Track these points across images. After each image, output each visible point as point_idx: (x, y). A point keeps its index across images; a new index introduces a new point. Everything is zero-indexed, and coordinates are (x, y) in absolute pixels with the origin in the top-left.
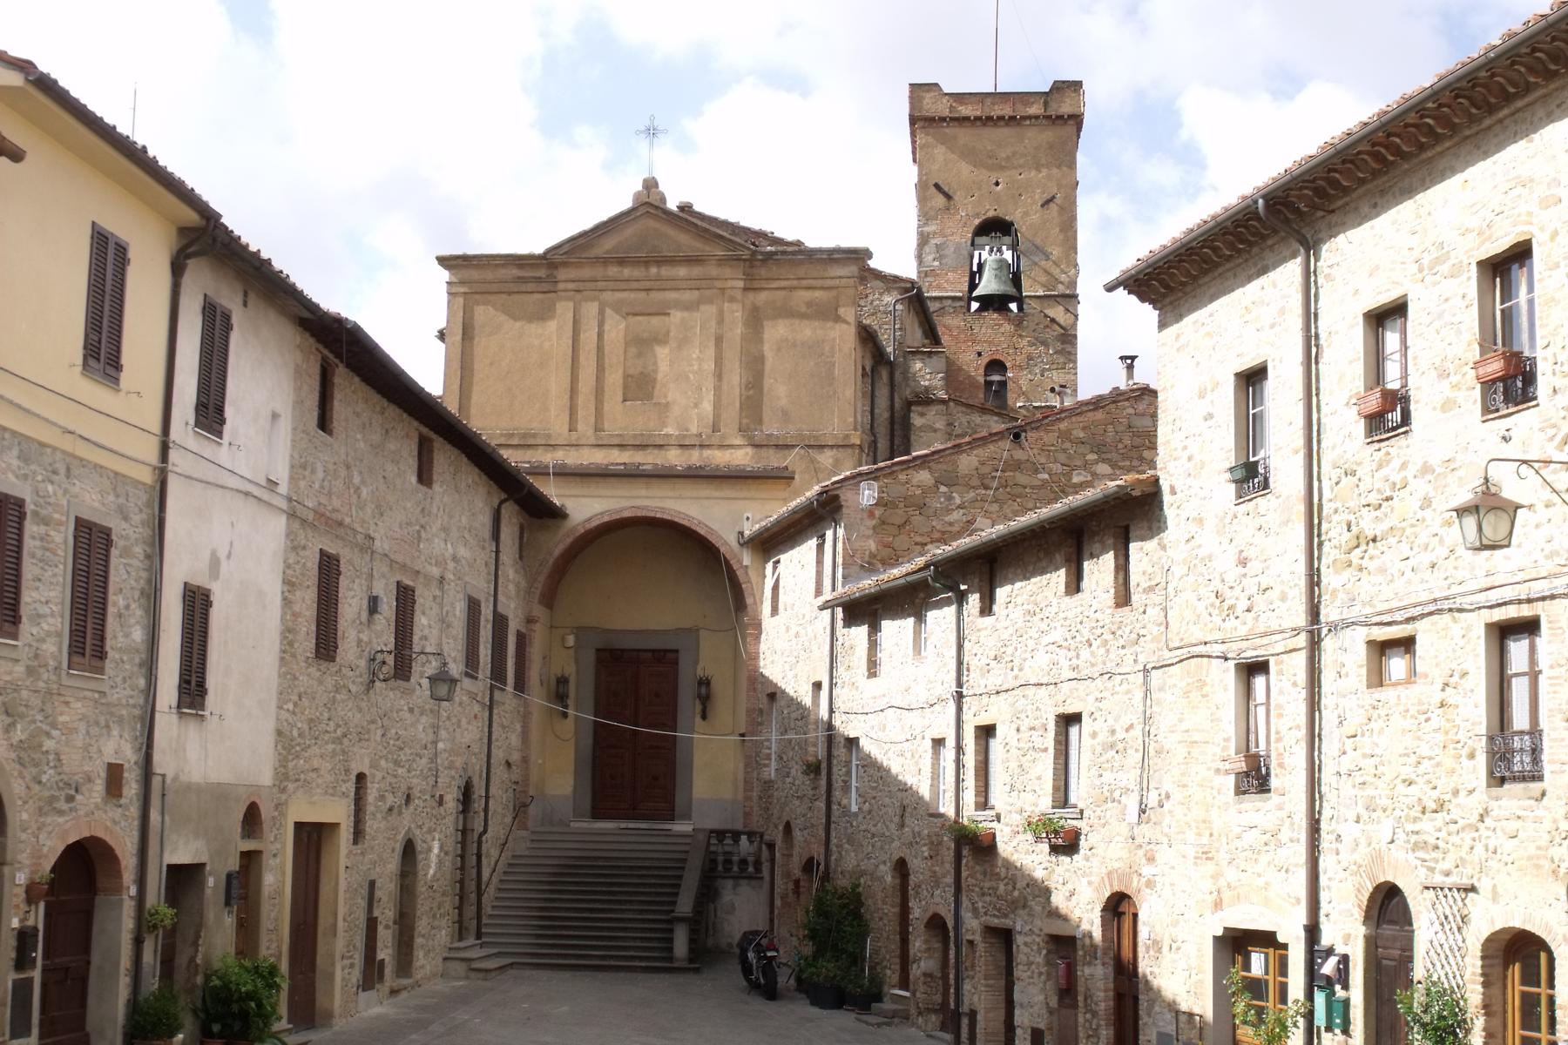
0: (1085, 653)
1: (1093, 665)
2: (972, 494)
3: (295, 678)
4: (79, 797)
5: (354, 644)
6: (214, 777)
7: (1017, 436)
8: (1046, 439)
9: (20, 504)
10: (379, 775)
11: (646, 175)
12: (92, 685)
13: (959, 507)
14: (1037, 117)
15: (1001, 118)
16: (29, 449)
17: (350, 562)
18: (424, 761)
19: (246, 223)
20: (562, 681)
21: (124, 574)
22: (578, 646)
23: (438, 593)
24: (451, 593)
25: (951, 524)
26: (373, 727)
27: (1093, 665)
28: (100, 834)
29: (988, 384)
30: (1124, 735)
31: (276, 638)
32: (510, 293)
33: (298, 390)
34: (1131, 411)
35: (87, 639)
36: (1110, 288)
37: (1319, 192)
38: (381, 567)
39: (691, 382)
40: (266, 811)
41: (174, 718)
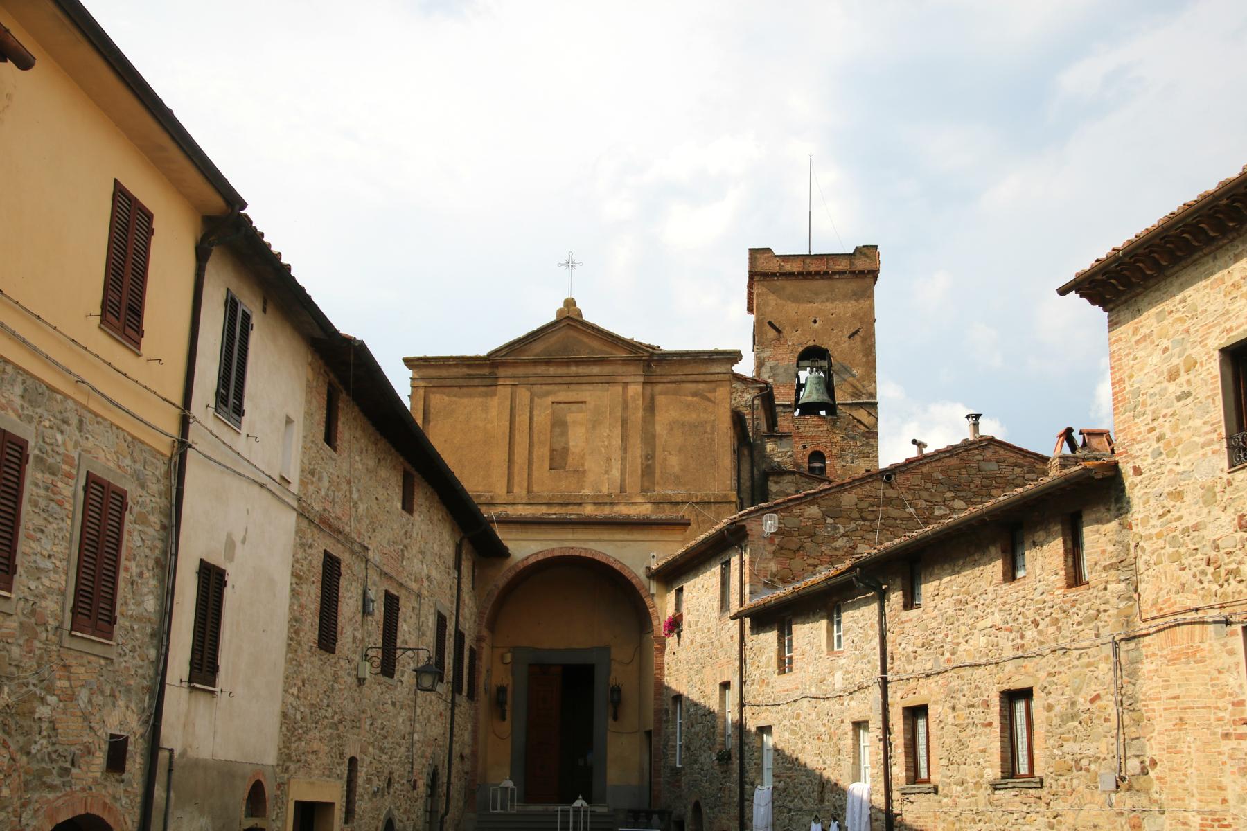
0: (1030, 633)
1: (1041, 643)
2: (853, 525)
3: (300, 665)
4: (75, 771)
5: (350, 640)
6: (222, 755)
7: (889, 477)
9: (22, 445)
10: (367, 760)
12: (98, 650)
13: (843, 535)
14: (843, 272)
15: (817, 273)
16: (36, 392)
17: (349, 566)
18: (403, 749)
19: (267, 217)
21: (138, 539)
23: (416, 605)
24: (426, 607)
25: (836, 549)
26: (363, 716)
27: (1041, 643)
28: (96, 811)
29: (811, 469)
30: (1088, 705)
31: (285, 626)
32: (460, 387)
33: (309, 402)
34: (979, 457)
35: (94, 604)
36: (1063, 291)
38: (373, 576)
39: (599, 451)
40: (270, 789)
41: (185, 693)
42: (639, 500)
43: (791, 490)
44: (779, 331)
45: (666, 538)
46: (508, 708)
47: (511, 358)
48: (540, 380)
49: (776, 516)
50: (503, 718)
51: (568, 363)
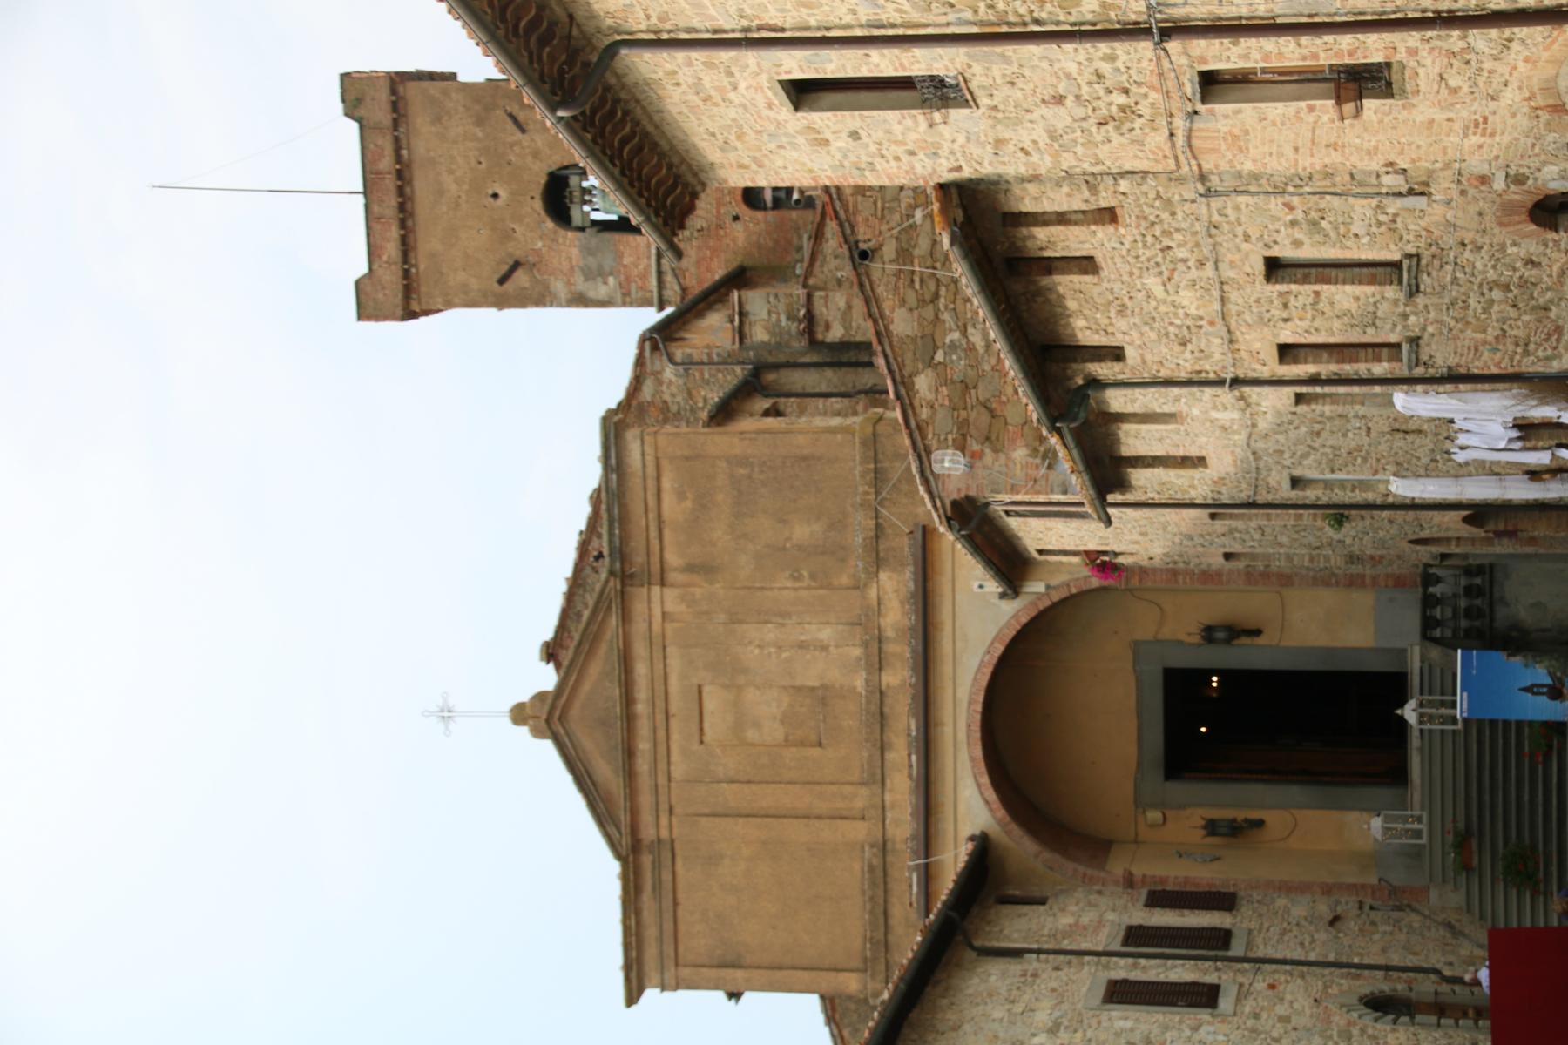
0: (1182, 253)
2: (946, 316)
7: (864, 255)
8: (866, 214)
11: (507, 721)
13: (964, 333)
15: (400, 191)
20: (1212, 827)
22: (1161, 805)
32: (676, 903)
37: (544, 41)
42: (873, 593)
43: (839, 299)
44: (516, 265)
45: (948, 566)
46: (1241, 815)
47: (624, 818)
48: (662, 766)
49: (936, 455)
50: (1260, 823)
51: (629, 718)
